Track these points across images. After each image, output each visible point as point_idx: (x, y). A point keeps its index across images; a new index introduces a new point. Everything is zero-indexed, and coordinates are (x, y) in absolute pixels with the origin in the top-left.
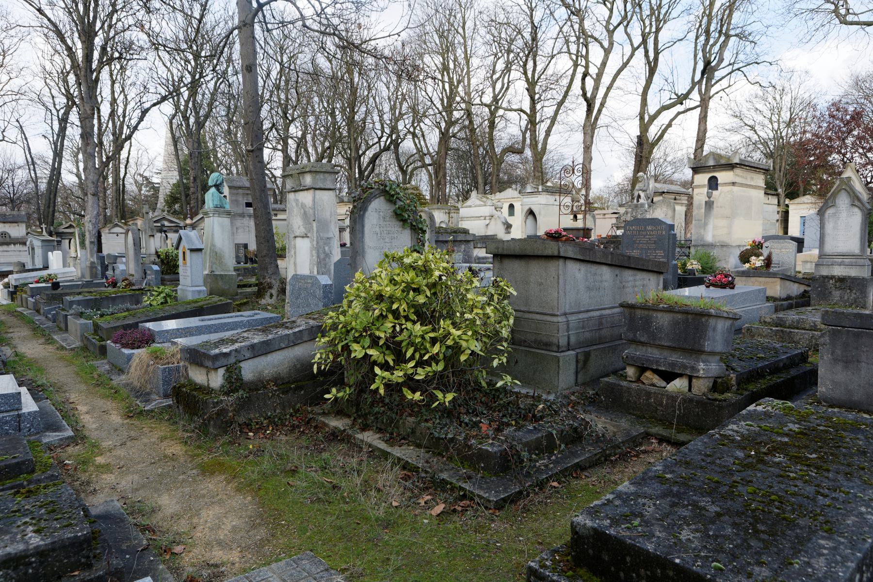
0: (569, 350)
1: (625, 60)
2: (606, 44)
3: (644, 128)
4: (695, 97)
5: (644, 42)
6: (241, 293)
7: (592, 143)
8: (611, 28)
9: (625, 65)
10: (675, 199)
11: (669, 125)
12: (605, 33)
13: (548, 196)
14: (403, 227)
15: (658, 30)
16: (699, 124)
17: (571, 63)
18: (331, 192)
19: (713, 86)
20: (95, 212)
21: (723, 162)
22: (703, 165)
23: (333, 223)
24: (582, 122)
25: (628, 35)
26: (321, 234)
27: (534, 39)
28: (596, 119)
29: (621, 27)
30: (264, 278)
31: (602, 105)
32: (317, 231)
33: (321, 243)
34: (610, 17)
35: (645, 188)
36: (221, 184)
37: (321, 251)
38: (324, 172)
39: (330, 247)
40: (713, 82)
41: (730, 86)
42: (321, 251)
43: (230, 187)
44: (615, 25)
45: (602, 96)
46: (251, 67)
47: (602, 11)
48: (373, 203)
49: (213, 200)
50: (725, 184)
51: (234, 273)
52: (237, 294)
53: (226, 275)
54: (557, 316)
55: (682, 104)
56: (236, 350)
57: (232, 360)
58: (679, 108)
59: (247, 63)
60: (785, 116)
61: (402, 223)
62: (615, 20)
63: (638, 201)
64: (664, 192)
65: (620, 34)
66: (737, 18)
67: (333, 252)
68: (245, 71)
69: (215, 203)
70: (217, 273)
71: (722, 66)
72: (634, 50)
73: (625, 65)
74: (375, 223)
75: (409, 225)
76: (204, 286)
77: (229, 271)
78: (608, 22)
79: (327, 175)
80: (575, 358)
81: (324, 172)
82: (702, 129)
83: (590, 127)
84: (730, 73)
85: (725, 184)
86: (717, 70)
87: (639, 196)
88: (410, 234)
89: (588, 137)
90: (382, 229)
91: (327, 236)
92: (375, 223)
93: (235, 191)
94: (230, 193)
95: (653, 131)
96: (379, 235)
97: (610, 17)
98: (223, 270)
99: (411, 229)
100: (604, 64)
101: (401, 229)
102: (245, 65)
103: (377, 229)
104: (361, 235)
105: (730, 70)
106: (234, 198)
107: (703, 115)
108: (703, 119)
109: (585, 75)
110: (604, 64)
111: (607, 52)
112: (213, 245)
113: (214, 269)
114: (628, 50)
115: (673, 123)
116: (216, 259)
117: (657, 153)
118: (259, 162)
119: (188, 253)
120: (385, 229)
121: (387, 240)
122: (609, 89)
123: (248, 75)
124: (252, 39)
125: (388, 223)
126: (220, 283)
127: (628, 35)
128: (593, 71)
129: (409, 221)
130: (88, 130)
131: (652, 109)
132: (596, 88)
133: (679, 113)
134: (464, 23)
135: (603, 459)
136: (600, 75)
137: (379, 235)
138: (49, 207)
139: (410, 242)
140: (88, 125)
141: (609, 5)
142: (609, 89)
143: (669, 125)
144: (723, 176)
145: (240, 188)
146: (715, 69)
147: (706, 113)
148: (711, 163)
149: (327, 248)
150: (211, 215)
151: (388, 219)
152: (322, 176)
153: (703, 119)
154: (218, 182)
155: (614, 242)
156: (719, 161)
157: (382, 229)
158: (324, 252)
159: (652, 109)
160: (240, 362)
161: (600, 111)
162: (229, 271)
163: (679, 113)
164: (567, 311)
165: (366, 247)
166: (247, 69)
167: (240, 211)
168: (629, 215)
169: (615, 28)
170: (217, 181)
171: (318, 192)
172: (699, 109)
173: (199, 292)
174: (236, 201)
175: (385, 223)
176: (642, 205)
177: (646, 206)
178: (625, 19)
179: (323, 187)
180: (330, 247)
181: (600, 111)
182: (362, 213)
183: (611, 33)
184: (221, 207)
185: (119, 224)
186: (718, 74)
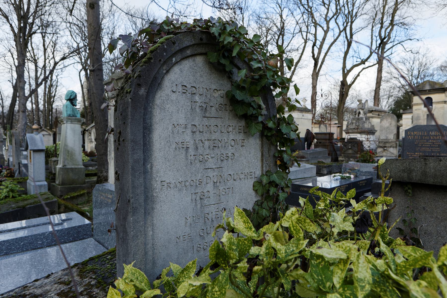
1: (335, 38)
2: (325, 28)
3: (345, 75)
4: (374, 59)
5: (345, 29)
6: (88, 182)
7: (316, 84)
8: (328, 19)
9: (335, 41)
10: (379, 115)
11: (358, 75)
12: (325, 22)
13: (299, 113)
14: (247, 132)
15: (352, 22)
16: (378, 74)
17: (303, 41)
19: (385, 52)
20: (24, 122)
21: (437, 87)
22: (421, 89)
24: (311, 73)
25: (337, 24)
27: (283, 28)
28: (319, 71)
29: (333, 19)
30: (102, 173)
31: (322, 63)
34: (327, 13)
35: (363, 108)
40: (385, 50)
41: (392, 54)
44: (330, 17)
45: (322, 58)
46: (93, 5)
47: (323, 10)
48: (176, 69)
49: (67, 111)
50: (439, 102)
51: (83, 167)
52: (85, 183)
53: (75, 168)
55: (364, 64)
58: (362, 66)
59: (91, 2)
60: (416, 72)
61: (243, 123)
62: (330, 14)
63: (359, 116)
64: (373, 111)
65: (332, 24)
66: (403, 11)
68: (89, 8)
69: (69, 113)
70: (68, 167)
71: (389, 42)
72: (340, 32)
73: (335, 41)
74: (182, 121)
75: (260, 127)
76: (46, 181)
77: (79, 165)
78: (326, 15)
82: (379, 76)
83: (315, 75)
84: (392, 47)
85: (439, 102)
86: (387, 44)
87: (359, 113)
88: (258, 147)
89: (315, 81)
92: (182, 121)
95: (349, 80)
96: (191, 152)
97: (327, 13)
98: (74, 164)
99: (262, 135)
100: (324, 39)
101: (241, 136)
102: (88, 3)
103: (188, 138)
104: (139, 154)
105: (392, 46)
107: (380, 69)
108: (380, 71)
109: (314, 45)
110: (324, 39)
111: (326, 32)
112: (66, 145)
113: (66, 164)
114: (337, 31)
115: (360, 74)
116: (68, 156)
117: (351, 92)
118: (99, 80)
119: (32, 152)
120: (206, 136)
121: (211, 163)
122: (326, 54)
123: (91, 11)
125: (213, 122)
126: (71, 174)
127: (337, 24)
128: (318, 43)
129: (260, 119)
130: (21, 73)
131: (348, 67)
132: (319, 53)
133: (364, 69)
134: (243, 19)
136: (321, 46)
137: (191, 152)
138: (9, 120)
139: (259, 164)
140: (21, 70)
141: (327, 6)
142: (326, 54)
143: (358, 75)
144: (435, 97)
146: (386, 43)
147: (382, 67)
148: (427, 87)
150: (65, 122)
151: (213, 112)
153: (380, 71)
154: (72, 97)
155: (351, 142)
156: (434, 86)
157: (198, 136)
159: (348, 67)
161: (321, 66)
162: (79, 165)
163: (364, 69)
165: (157, 185)
166: (90, 6)
168: (354, 125)
169: (331, 19)
170: (71, 96)
172: (377, 65)
173: (41, 186)
175: (206, 122)
176: (362, 118)
177: (364, 119)
178: (336, 14)
181: (321, 66)
182: (142, 91)
183: (328, 23)
184: (73, 116)
185: (45, 129)
186: (388, 46)
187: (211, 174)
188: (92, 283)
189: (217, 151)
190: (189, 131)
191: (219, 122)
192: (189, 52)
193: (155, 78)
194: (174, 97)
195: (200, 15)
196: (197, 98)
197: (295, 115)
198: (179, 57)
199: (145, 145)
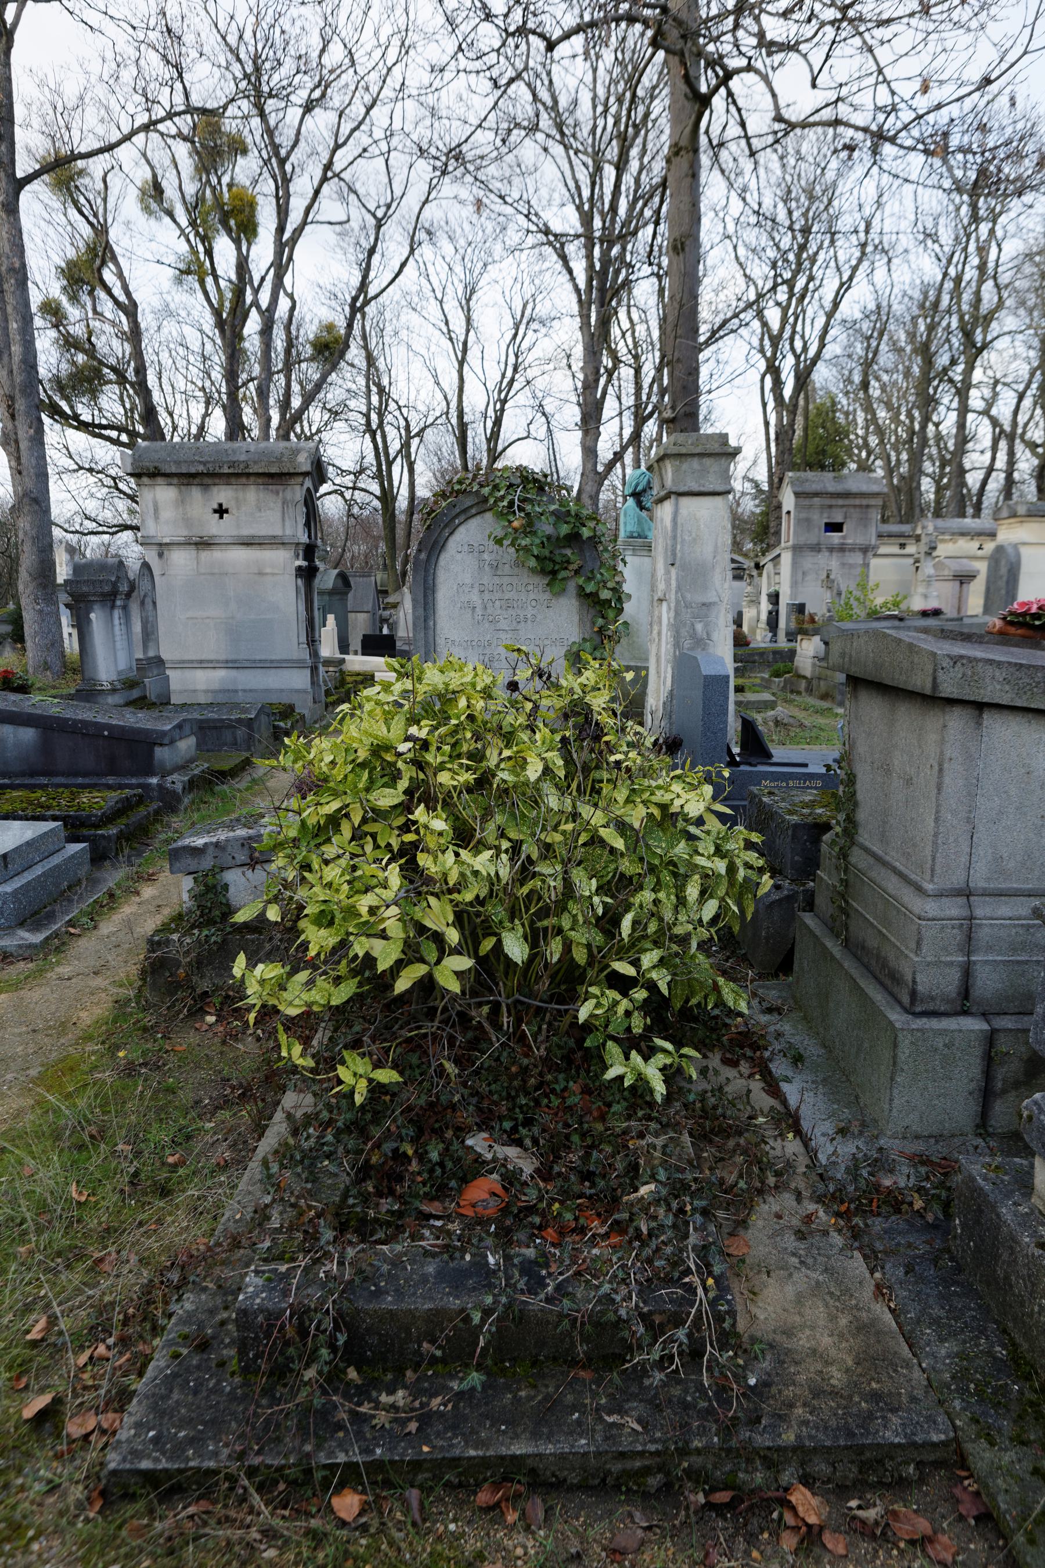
0: (965, 1013)
2: (845, 278)
18: (718, 501)
23: (718, 570)
26: (688, 596)
32: (679, 588)
33: (686, 615)
36: (644, 491)
37: (684, 632)
38: (701, 455)
39: (706, 625)
42: (684, 632)
43: (797, 495)
48: (462, 529)
54: (919, 889)
56: (217, 845)
57: (207, 863)
67: (715, 636)
79: (707, 461)
80: (978, 1051)
81: (701, 455)
90: (487, 596)
91: (700, 598)
93: (807, 502)
94: (796, 505)
96: (479, 611)
101: (547, 596)
103: (475, 598)
106: (803, 515)
120: (498, 595)
121: (503, 624)
123: (675, 258)
124: (689, 179)
125: (506, 580)
135: (654, 1482)
145: (816, 494)
149: (699, 627)
152: (695, 463)
157: (487, 596)
158: (693, 635)
160: (222, 869)
164: (979, 881)
167: (813, 539)
171: (685, 501)
174: (808, 520)
175: (497, 581)
179: (696, 488)
180: (706, 625)
184: (639, 536)
187: (503, 636)
188: (979, 330)
189: (510, 611)
190: (476, 591)
191: (515, 581)
192: (474, 511)
193: (436, 542)
194: (459, 557)
195: (83, 324)
196: (486, 556)
197: (718, 101)
198: (462, 518)
199: (426, 604)
